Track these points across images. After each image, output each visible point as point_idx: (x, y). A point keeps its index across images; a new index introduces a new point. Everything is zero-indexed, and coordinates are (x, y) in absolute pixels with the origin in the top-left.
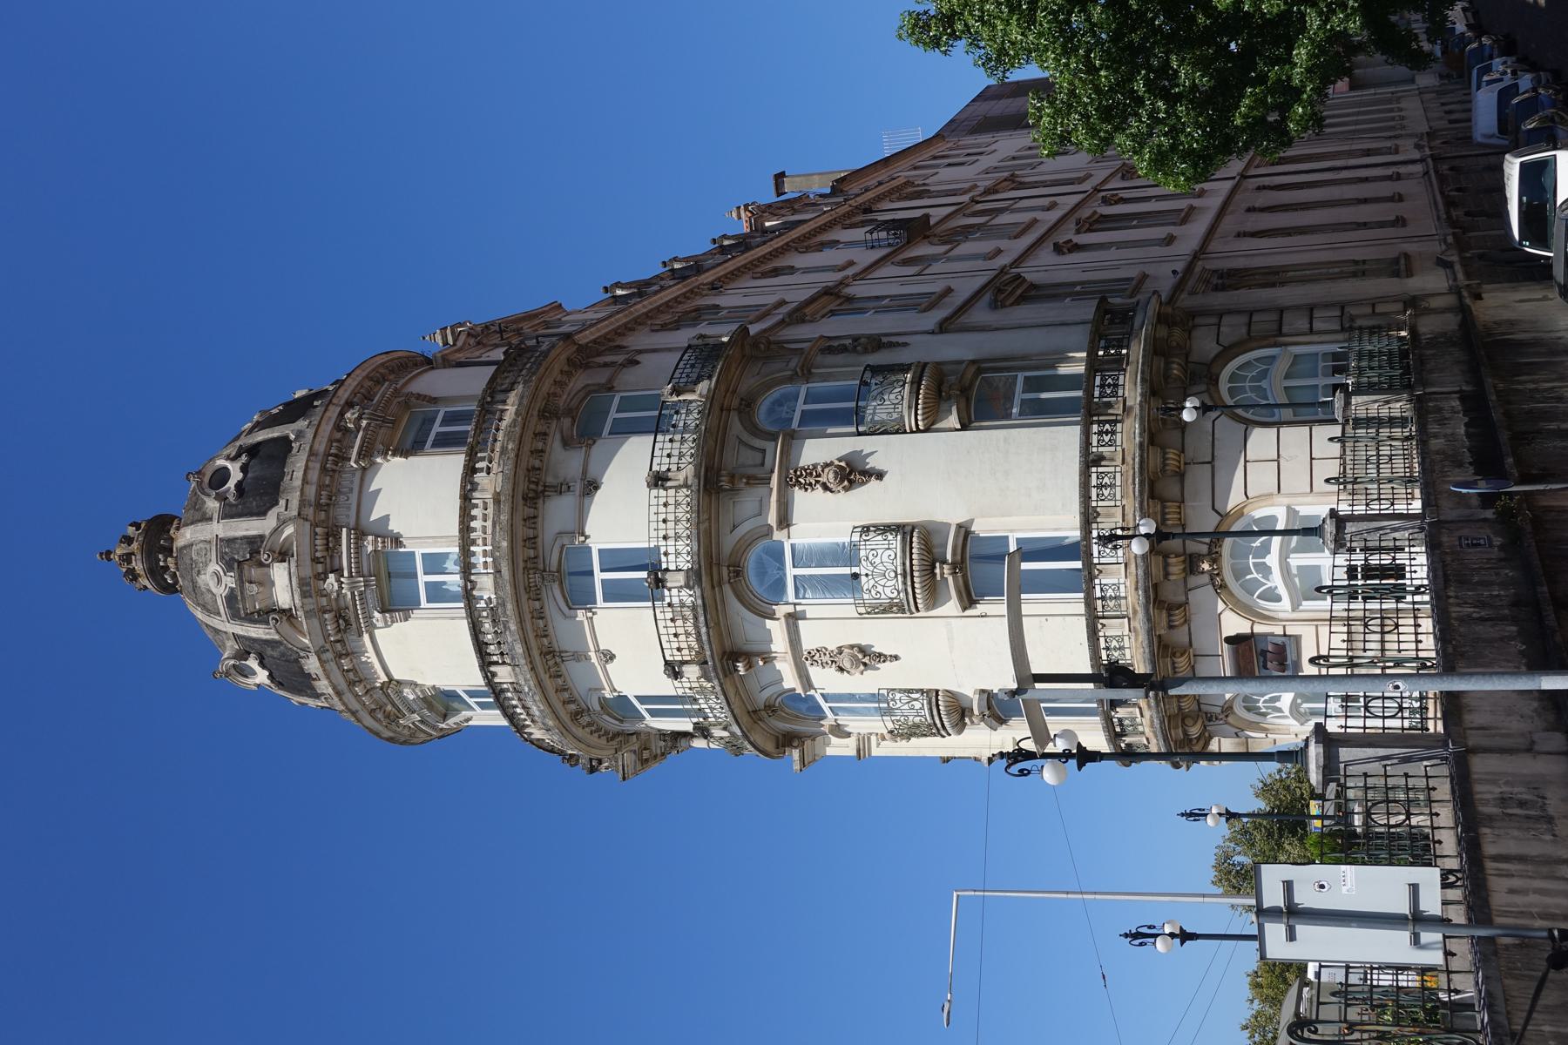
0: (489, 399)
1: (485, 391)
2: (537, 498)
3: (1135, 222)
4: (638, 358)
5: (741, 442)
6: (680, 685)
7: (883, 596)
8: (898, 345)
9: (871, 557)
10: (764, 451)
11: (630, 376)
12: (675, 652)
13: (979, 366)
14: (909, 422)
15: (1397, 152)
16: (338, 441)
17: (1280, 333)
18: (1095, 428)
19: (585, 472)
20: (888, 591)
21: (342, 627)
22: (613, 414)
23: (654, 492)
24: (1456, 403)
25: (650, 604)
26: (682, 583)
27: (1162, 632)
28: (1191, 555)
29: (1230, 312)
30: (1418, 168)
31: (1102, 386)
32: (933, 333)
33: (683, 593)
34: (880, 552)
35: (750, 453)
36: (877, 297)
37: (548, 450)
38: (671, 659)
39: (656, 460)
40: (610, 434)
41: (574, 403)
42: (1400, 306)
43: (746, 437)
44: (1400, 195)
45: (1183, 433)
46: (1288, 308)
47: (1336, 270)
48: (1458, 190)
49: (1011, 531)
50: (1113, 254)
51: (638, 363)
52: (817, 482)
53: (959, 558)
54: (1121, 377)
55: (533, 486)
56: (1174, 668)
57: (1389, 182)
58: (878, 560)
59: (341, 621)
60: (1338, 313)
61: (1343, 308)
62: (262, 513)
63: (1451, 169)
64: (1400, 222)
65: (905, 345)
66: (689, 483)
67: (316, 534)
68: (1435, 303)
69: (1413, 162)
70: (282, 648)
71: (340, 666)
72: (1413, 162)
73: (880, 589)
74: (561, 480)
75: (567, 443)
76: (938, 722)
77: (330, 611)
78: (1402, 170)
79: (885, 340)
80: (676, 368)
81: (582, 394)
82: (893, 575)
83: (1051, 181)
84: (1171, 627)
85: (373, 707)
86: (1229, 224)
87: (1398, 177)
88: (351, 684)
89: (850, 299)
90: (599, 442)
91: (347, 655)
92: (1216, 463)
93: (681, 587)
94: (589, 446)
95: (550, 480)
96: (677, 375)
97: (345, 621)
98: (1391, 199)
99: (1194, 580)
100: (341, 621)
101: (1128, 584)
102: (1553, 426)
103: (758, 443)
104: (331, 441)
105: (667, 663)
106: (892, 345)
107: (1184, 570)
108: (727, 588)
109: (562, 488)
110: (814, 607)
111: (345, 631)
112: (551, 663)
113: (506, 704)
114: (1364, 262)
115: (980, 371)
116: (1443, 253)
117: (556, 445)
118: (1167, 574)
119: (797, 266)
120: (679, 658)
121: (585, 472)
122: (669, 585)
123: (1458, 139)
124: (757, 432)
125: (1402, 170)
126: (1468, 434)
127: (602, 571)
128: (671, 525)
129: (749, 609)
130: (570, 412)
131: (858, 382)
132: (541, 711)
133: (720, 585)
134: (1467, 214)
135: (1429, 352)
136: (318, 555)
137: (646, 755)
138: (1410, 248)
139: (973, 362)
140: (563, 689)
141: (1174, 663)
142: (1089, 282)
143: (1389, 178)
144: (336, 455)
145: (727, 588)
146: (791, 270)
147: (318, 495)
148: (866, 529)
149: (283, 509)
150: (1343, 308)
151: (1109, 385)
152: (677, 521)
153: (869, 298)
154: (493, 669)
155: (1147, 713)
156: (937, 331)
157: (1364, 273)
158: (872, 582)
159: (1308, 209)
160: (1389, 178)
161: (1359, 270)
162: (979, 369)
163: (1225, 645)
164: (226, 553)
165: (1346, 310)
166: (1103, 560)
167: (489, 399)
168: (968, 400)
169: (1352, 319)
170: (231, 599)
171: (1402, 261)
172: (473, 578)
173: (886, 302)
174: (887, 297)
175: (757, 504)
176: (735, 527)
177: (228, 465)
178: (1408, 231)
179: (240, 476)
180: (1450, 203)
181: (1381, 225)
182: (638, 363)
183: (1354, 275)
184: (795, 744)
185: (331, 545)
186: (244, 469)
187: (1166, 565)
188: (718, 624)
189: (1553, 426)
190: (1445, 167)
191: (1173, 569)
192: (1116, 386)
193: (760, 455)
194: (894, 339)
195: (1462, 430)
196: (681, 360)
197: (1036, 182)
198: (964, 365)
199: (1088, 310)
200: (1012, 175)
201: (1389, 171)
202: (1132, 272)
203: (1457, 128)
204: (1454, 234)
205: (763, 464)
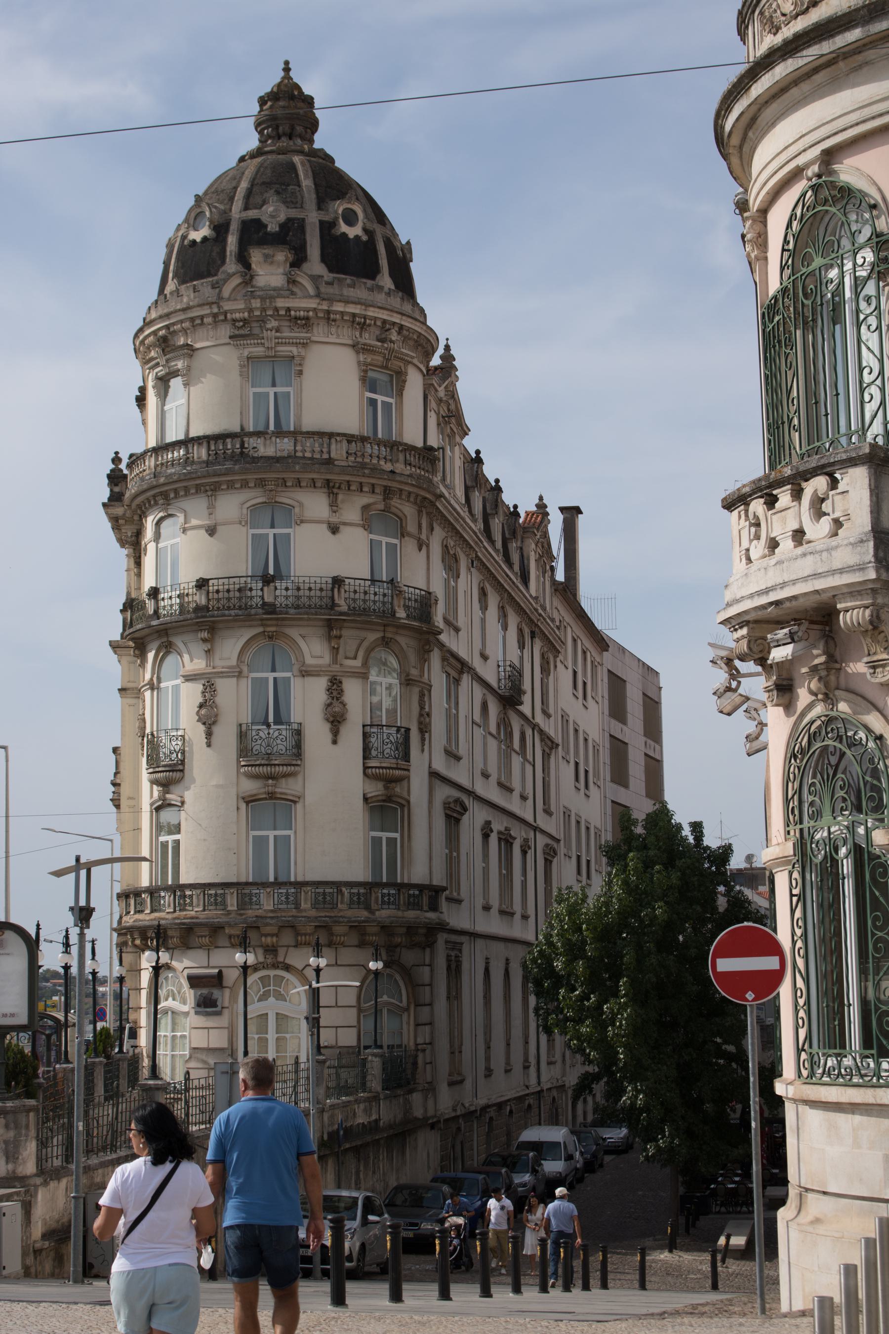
0: (400, 449)
1: (406, 444)
2: (329, 487)
3: (504, 872)
4: (424, 548)
5: (363, 641)
6: (190, 586)
7: (254, 744)
8: (423, 745)
9: (281, 737)
10: (355, 658)
11: (410, 545)
12: (216, 588)
13: (405, 805)
14: (372, 763)
15: (549, 1063)
16: (375, 323)
17: (417, 1005)
18: (362, 891)
19: (345, 524)
20: (258, 747)
21: (237, 324)
22: (385, 540)
23: (330, 581)
24: (374, 1117)
25: (250, 574)
26: (266, 600)
27: (227, 931)
28: (276, 951)
29: (432, 971)
30: (533, 1080)
31: (389, 894)
32: (430, 767)
33: (259, 600)
34: (285, 743)
35: (354, 647)
36: (457, 703)
37: (362, 494)
38: (211, 584)
39: (352, 581)
40: (371, 540)
41: (393, 510)
42: (429, 1079)
43: (366, 644)
44: (510, 1070)
45: (356, 946)
46: (432, 1009)
47: (456, 1034)
48: (511, 1112)
49: (295, 832)
50: (479, 864)
51: (420, 550)
52: (333, 699)
53: (279, 796)
54: (394, 907)
55: (337, 485)
56: (202, 936)
57: (522, 1059)
58: (279, 741)
59: (241, 324)
60: (427, 1041)
61: (430, 1044)
62: (324, 259)
63: (530, 1106)
64: (489, 1073)
65: (423, 751)
66: (336, 608)
67: (308, 312)
68: (430, 1102)
69: (539, 1077)
70: (219, 262)
71: (207, 315)
72: (539, 1077)
73: (259, 742)
74: (340, 505)
75: (365, 508)
76: (160, 769)
77: (249, 316)
78: (533, 1070)
79: (427, 735)
80: (415, 588)
81: (400, 514)
82: (269, 752)
83: (549, 782)
84: (230, 937)
85: (172, 329)
86: (499, 951)
87: (526, 1067)
88: (192, 320)
89: (457, 681)
90: (365, 533)
91: (215, 322)
92: (335, 968)
93: (263, 599)
94: (363, 527)
95: (340, 497)
96: (411, 590)
97: (242, 327)
98: (508, 1063)
99: (260, 951)
100: (241, 324)
101: (260, 911)
102: (362, 1168)
103: (361, 654)
104: (376, 319)
105: (208, 580)
106: (423, 740)
107: (268, 946)
108: (261, 629)
109: (334, 506)
110: (246, 686)
111: (234, 325)
112: (208, 488)
113: (177, 448)
114: (460, 1052)
115: (402, 806)
116: (463, 1104)
117: (366, 500)
118: (266, 935)
119: (487, 612)
120: (211, 588)
121: (345, 524)
122: (266, 589)
123: (557, 1110)
124: (369, 651)
125: (533, 1070)
126: (359, 1124)
127: (274, 534)
128: (307, 593)
129: (246, 642)
130: (387, 509)
131: (399, 725)
132: (171, 474)
133: (262, 625)
134: (491, 1119)
135: (401, 1100)
136: (293, 313)
137: (121, 522)
138: (468, 1084)
139: (409, 802)
140: (187, 489)
141: (205, 936)
142: (459, 862)
143: (526, 1060)
144: (365, 323)
145: (261, 629)
146: (484, 608)
147: (336, 312)
148: (298, 733)
149: (326, 278)
150: (430, 1044)
151: (389, 899)
152: (310, 597)
153: (457, 698)
154: (205, 444)
155: (170, 916)
156: (432, 770)
157: (452, 1053)
158: (264, 737)
159: (505, 998)
160: (526, 1060)
161: (455, 1051)
162: (404, 806)
163: (217, 971)
164: (293, 224)
165: (429, 1046)
166: (276, 895)
167: (400, 449)
168: (384, 801)
169: (424, 1051)
170: (257, 224)
171: (459, 1078)
172: (274, 439)
173: (454, 711)
174: (457, 710)
175: (319, 655)
176: (303, 637)
177: (360, 225)
178: (481, 1080)
179: (351, 236)
180: (500, 1106)
181: (488, 1059)
182: (420, 550)
183: (452, 1046)
184: (137, 652)
185: (299, 322)
186: (357, 237)
187: (272, 935)
188: (235, 621)
189: (362, 1168)
190: (532, 1101)
191: (269, 939)
192: (389, 903)
193: (352, 655)
194: (427, 742)
195: (361, 1121)
196: (421, 590)
197: (549, 768)
198: (406, 797)
199: (439, 879)
200: (557, 745)
201: (532, 1060)
202: (464, 893)
203: (567, 1109)
204: (476, 1111)
205: (347, 658)
